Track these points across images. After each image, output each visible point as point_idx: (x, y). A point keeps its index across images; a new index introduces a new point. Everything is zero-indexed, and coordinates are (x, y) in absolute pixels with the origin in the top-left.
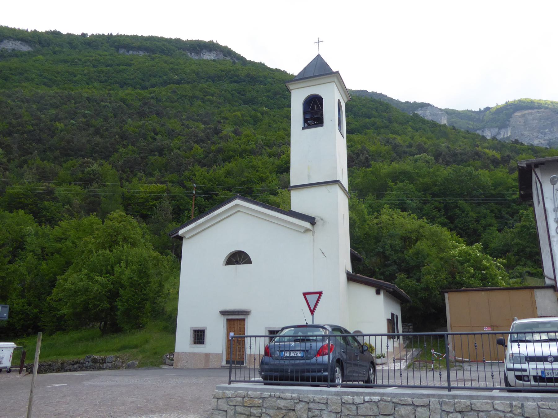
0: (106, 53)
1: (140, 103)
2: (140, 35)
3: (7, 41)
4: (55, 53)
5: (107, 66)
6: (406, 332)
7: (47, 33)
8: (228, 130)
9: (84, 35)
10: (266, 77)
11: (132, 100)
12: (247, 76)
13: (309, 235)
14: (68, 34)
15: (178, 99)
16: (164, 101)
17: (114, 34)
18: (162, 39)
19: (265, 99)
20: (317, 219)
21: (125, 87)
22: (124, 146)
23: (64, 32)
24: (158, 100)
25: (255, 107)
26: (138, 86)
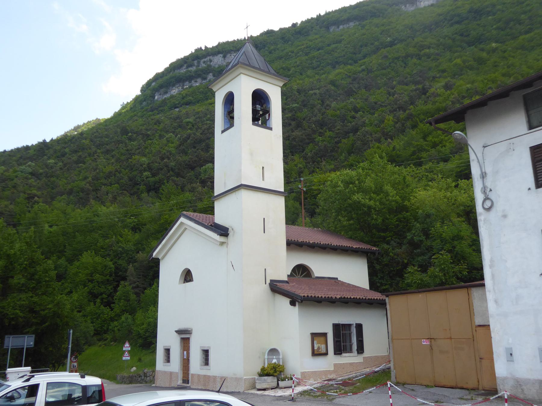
0: (317, 36)
1: (349, 80)
2: (347, 5)
3: (229, 55)
4: (270, 53)
5: (319, 50)
6: (351, 346)
7: (262, 35)
8: (437, 87)
9: (294, 25)
10: (494, 6)
11: (342, 79)
12: (470, 12)
13: (225, 246)
14: (281, 30)
15: (390, 63)
16: (375, 71)
17: (322, 13)
18: (228, 43)
19: (494, 32)
20: (230, 229)
21: (337, 66)
22: (321, 135)
23: (276, 29)
24: (369, 71)
25: (481, 46)
26: (350, 61)
